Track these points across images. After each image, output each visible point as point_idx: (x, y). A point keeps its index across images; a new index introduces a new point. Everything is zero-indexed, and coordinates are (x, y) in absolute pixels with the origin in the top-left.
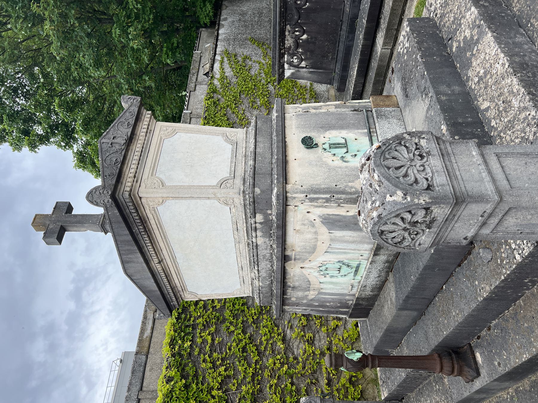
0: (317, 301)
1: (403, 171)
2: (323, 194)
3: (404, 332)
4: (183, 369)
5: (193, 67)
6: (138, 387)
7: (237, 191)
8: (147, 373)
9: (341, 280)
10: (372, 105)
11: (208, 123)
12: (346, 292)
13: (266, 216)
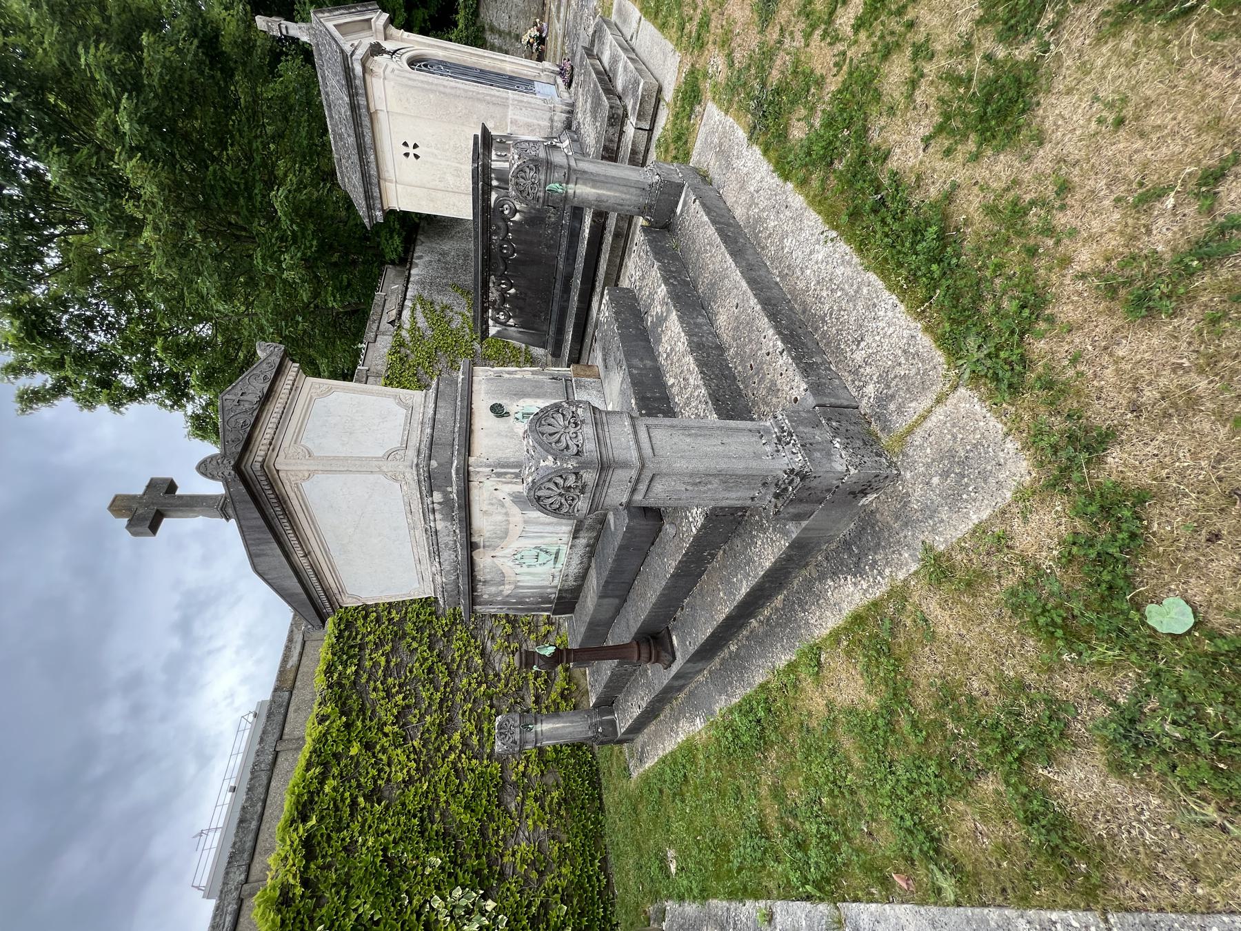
0: (514, 597)
1: (557, 436)
3: (609, 623)
4: (344, 704)
5: (374, 312)
6: (276, 736)
7: (408, 463)
8: (291, 715)
9: (539, 569)
11: (391, 384)
12: (546, 583)
13: (446, 494)
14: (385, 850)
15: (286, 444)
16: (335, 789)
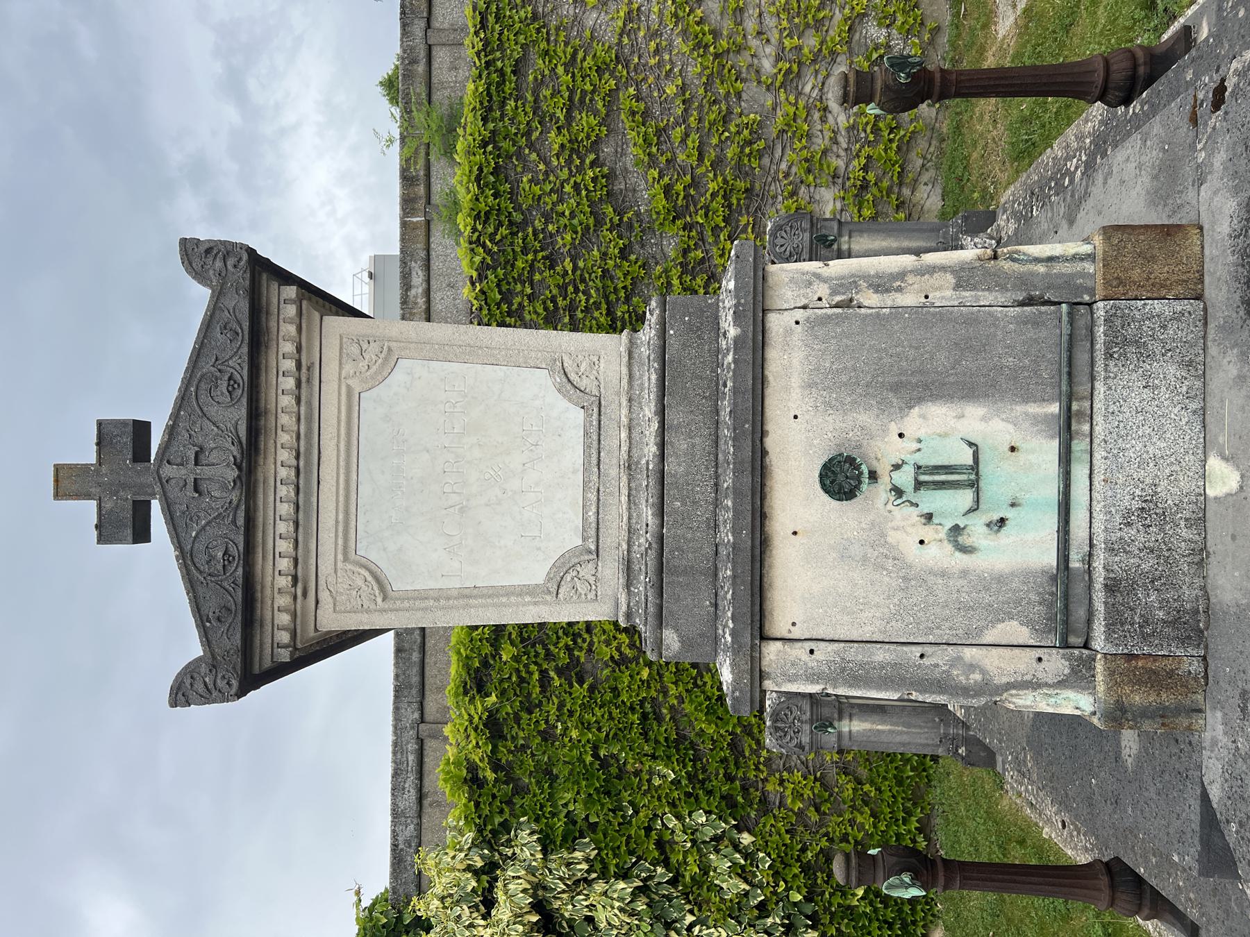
2: (879, 688)
10: (1099, 277)
14: (595, 748)
15: (326, 567)
16: (516, 659)
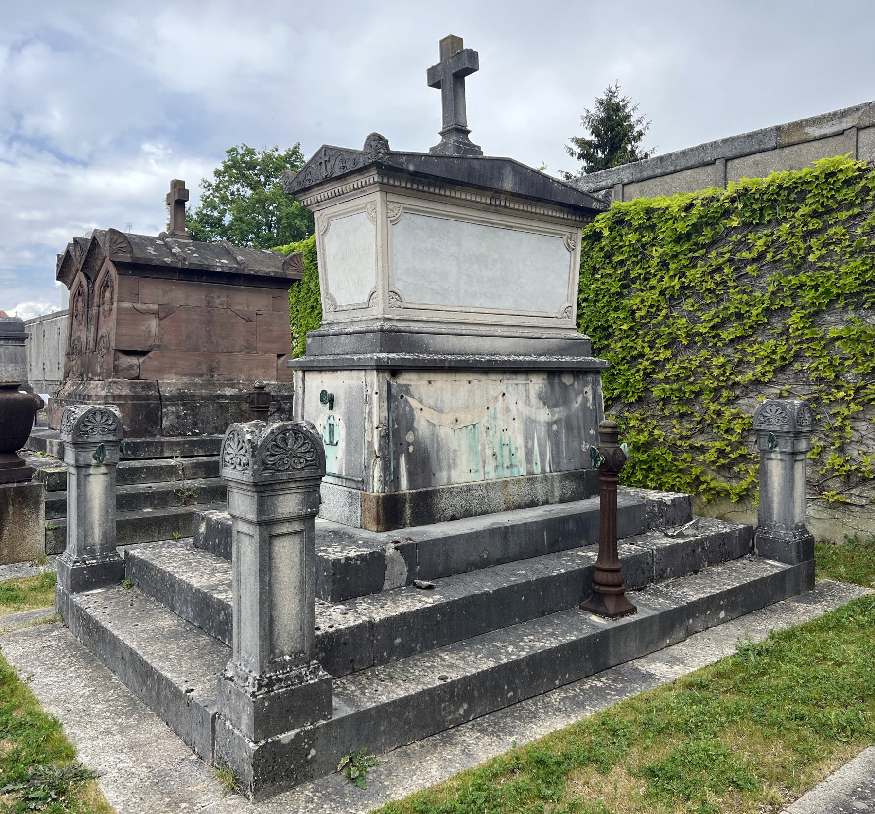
6: (729, 154)
